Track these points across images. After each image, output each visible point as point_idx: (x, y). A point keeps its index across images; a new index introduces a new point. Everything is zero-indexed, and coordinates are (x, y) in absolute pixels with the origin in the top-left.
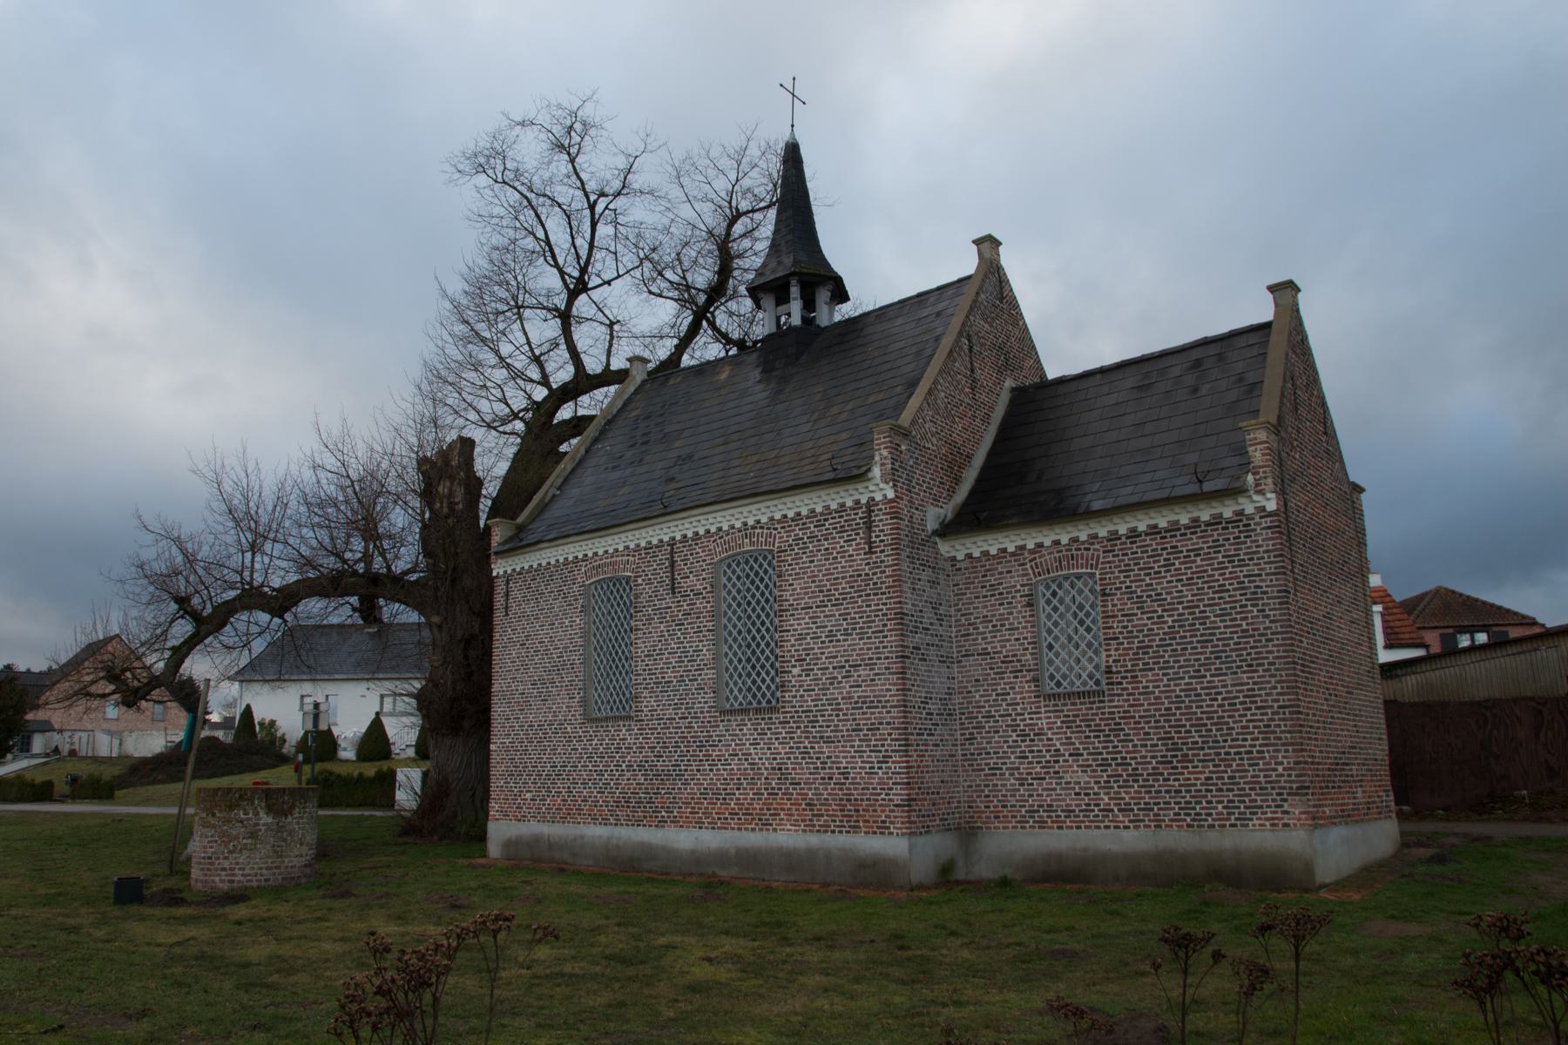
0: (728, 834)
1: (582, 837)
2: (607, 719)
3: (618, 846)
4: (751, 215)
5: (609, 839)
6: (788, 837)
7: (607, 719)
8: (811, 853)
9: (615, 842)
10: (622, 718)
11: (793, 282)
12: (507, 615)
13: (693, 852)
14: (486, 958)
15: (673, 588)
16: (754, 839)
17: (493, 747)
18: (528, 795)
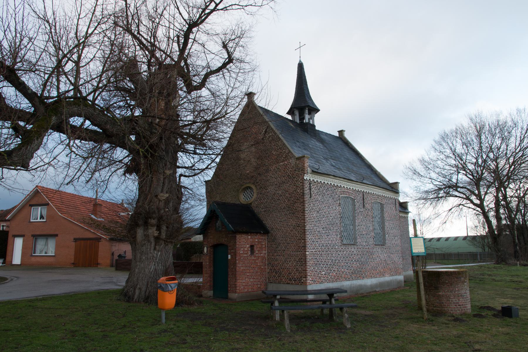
0: (377, 279)
1: (343, 286)
2: (348, 244)
3: (353, 287)
4: (84, 85)
5: (351, 285)
6: (387, 278)
7: (348, 244)
8: (391, 281)
9: (352, 286)
10: (353, 245)
11: (307, 108)
12: (311, 198)
13: (371, 285)
14: (165, 9)
15: (364, 206)
16: (382, 279)
17: (307, 253)
18: (323, 273)
